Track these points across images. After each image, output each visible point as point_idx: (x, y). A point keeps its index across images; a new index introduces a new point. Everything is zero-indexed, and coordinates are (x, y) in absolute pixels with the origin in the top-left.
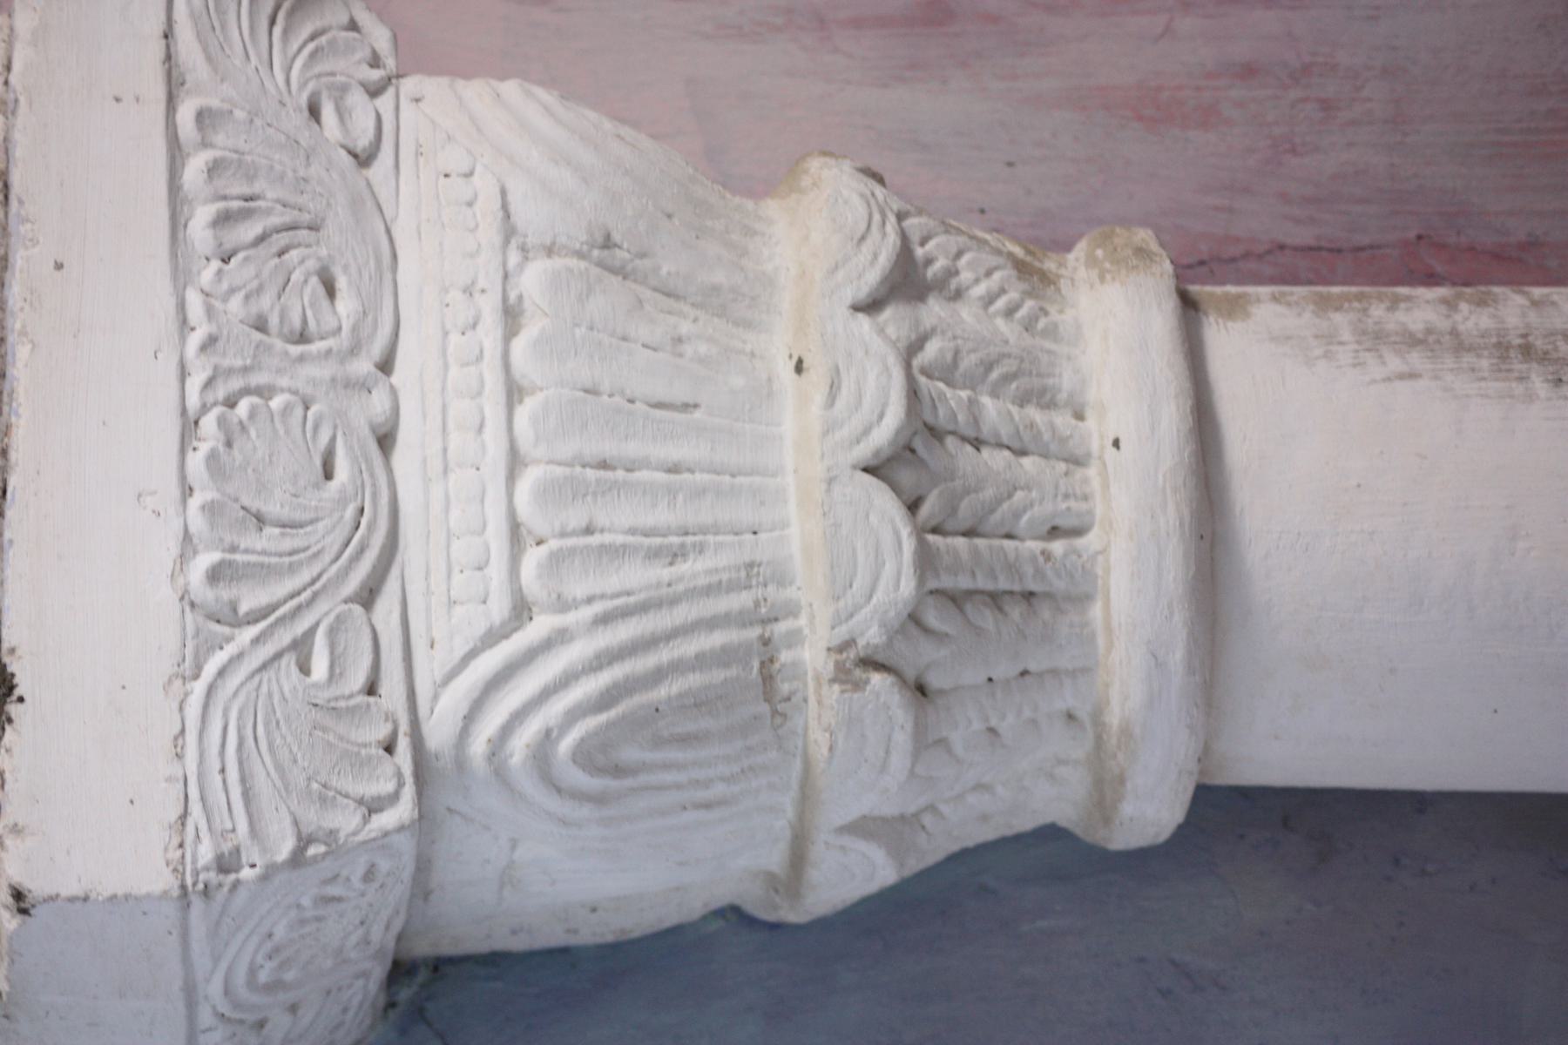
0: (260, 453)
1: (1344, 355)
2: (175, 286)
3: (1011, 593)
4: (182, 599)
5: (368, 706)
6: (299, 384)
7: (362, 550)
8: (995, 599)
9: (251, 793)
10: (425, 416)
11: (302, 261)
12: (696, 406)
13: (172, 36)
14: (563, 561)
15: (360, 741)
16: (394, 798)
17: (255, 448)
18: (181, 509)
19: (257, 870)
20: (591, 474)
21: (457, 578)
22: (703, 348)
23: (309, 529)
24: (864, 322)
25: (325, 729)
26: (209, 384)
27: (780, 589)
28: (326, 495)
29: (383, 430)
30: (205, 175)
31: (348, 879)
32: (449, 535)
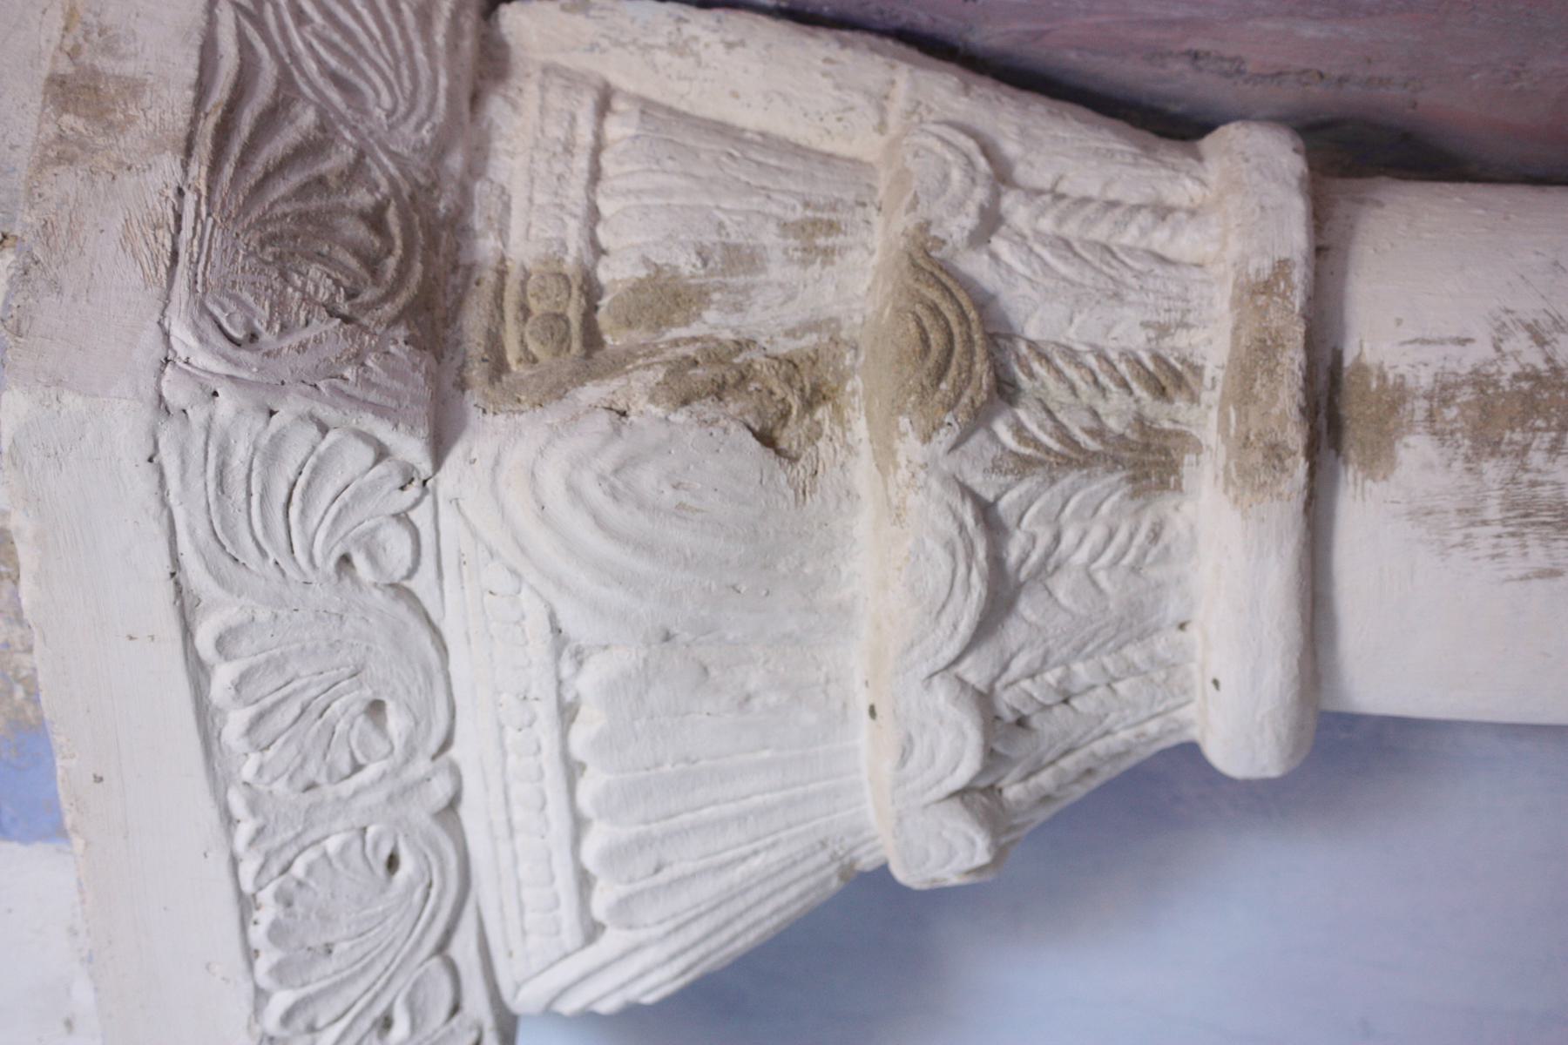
7: (433, 916)
10: (487, 789)
17: (316, 894)
22: (772, 699)
30: (233, 692)
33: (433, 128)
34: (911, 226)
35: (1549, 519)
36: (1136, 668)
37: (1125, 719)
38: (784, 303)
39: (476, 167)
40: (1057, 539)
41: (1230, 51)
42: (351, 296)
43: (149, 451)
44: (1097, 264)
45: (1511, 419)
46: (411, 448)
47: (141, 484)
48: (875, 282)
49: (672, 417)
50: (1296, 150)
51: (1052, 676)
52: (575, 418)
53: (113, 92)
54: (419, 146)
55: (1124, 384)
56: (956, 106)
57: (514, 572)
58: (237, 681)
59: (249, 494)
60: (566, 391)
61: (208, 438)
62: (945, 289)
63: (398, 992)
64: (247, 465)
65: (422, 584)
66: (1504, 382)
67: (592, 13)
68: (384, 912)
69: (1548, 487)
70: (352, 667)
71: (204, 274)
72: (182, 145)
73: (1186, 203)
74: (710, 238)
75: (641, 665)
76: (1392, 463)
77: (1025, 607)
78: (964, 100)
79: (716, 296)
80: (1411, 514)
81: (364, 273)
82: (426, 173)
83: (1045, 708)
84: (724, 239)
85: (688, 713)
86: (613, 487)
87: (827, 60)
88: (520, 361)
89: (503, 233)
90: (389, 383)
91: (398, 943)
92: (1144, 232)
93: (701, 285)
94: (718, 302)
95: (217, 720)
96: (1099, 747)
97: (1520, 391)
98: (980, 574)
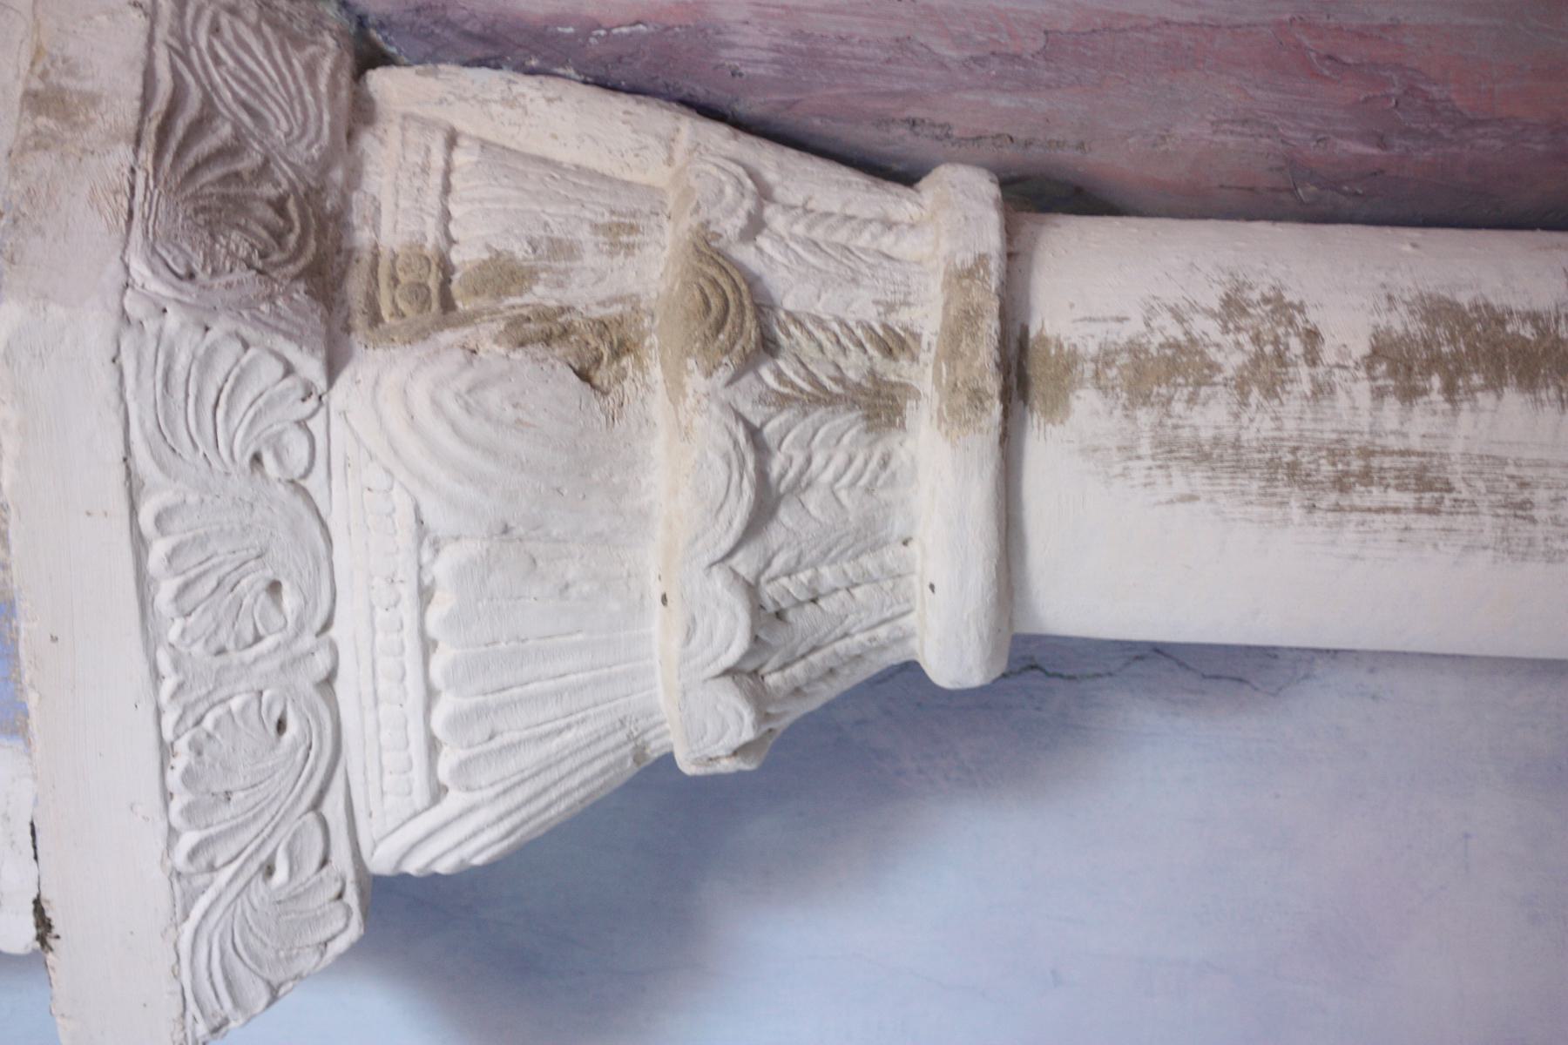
1: (1138, 469)
2: (147, 655)
7: (311, 775)
17: (220, 746)
22: (586, 588)
33: (321, 148)
34: (695, 224)
35: (1188, 455)
36: (870, 575)
37: (860, 621)
38: (596, 282)
39: (355, 176)
40: (809, 461)
41: (941, 118)
42: (263, 256)
43: (113, 352)
44: (839, 257)
45: (1158, 378)
46: (311, 367)
47: (105, 380)
48: (666, 269)
49: (512, 355)
50: (992, 181)
51: (804, 576)
52: (437, 352)
53: (76, 101)
54: (310, 159)
55: (860, 345)
56: (728, 147)
57: (388, 472)
58: (169, 553)
59: (187, 395)
60: (429, 334)
61: (158, 344)
62: (722, 268)
63: (281, 840)
64: (186, 371)
65: (314, 484)
66: (1153, 350)
67: (441, 76)
68: (273, 766)
69: (1187, 429)
70: (258, 549)
71: (154, 227)
72: (133, 137)
73: (907, 219)
74: (538, 233)
75: (484, 554)
76: (1067, 411)
77: (785, 515)
78: (733, 143)
79: (543, 275)
80: (1082, 451)
81: (272, 242)
82: (316, 179)
83: (799, 604)
84: (549, 234)
85: (519, 598)
86: (467, 403)
87: (626, 112)
88: (392, 315)
89: (376, 228)
90: (294, 318)
91: (283, 796)
92: (874, 237)
93: (531, 267)
94: (545, 280)
95: (152, 588)
96: (840, 646)
97: (1165, 356)
98: (750, 481)
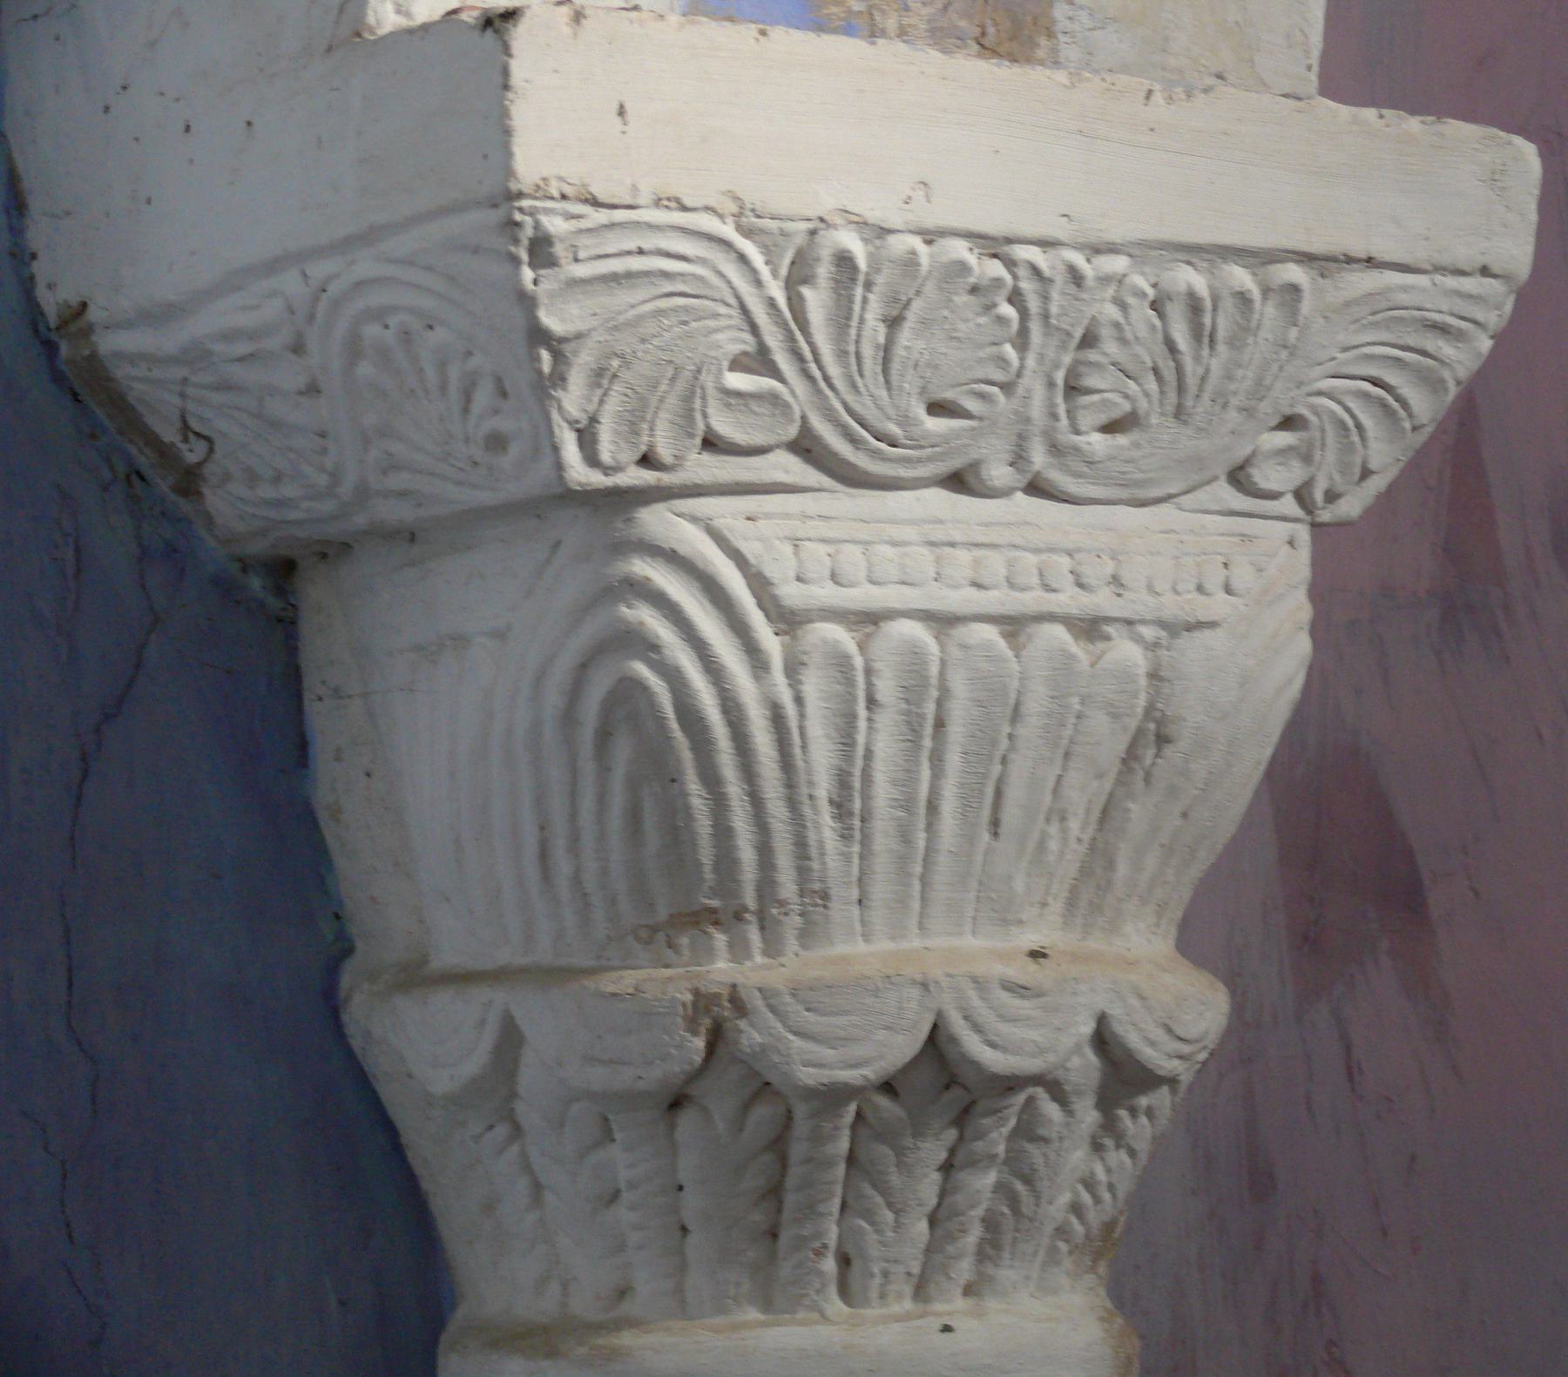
0: (962, 326)
3: (779, 1211)
4: (822, 220)
5: (691, 436)
6: (1025, 381)
8: (774, 1192)
9: (613, 284)
10: (987, 525)
11: (1147, 395)
12: (996, 834)
13: (1367, 267)
14: (842, 672)
15: (658, 422)
16: (592, 460)
18: (912, 229)
19: (529, 286)
20: (930, 709)
21: (822, 549)
23: (881, 379)
24: (1087, 1028)
25: (673, 380)
26: (1035, 271)
27: (797, 931)
28: (914, 401)
29: (971, 479)
30: (1238, 289)
31: (496, 412)
32: (866, 543)
43: (1496, 269)
47: (1464, 252)
